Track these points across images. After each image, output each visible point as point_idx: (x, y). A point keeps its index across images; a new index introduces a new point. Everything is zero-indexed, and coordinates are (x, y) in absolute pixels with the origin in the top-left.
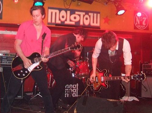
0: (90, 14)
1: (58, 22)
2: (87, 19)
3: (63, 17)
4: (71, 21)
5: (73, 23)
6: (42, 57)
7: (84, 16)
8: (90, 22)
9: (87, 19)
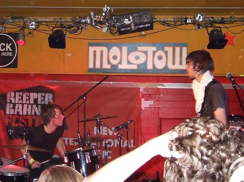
0: (166, 49)
1: (106, 66)
2: (160, 58)
3: (115, 57)
4: (129, 63)
5: (135, 67)
6: (209, 172)
7: (154, 53)
8: (132, 64)
9: (115, 57)
